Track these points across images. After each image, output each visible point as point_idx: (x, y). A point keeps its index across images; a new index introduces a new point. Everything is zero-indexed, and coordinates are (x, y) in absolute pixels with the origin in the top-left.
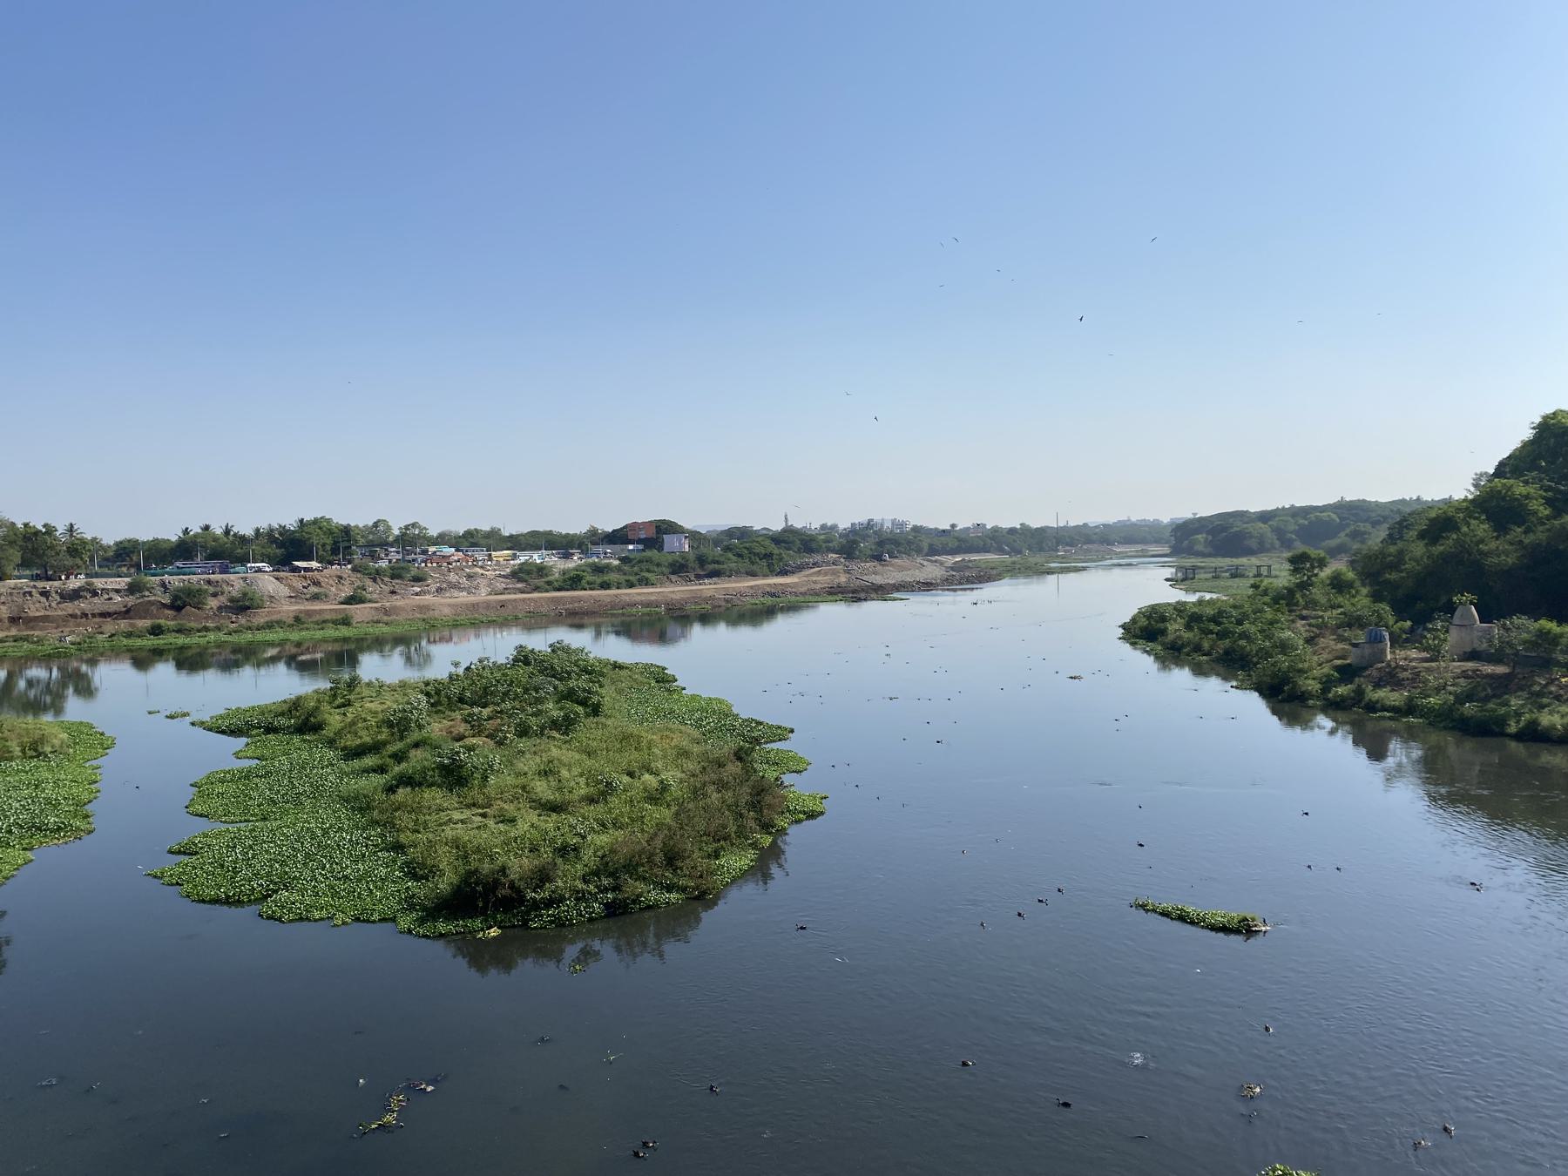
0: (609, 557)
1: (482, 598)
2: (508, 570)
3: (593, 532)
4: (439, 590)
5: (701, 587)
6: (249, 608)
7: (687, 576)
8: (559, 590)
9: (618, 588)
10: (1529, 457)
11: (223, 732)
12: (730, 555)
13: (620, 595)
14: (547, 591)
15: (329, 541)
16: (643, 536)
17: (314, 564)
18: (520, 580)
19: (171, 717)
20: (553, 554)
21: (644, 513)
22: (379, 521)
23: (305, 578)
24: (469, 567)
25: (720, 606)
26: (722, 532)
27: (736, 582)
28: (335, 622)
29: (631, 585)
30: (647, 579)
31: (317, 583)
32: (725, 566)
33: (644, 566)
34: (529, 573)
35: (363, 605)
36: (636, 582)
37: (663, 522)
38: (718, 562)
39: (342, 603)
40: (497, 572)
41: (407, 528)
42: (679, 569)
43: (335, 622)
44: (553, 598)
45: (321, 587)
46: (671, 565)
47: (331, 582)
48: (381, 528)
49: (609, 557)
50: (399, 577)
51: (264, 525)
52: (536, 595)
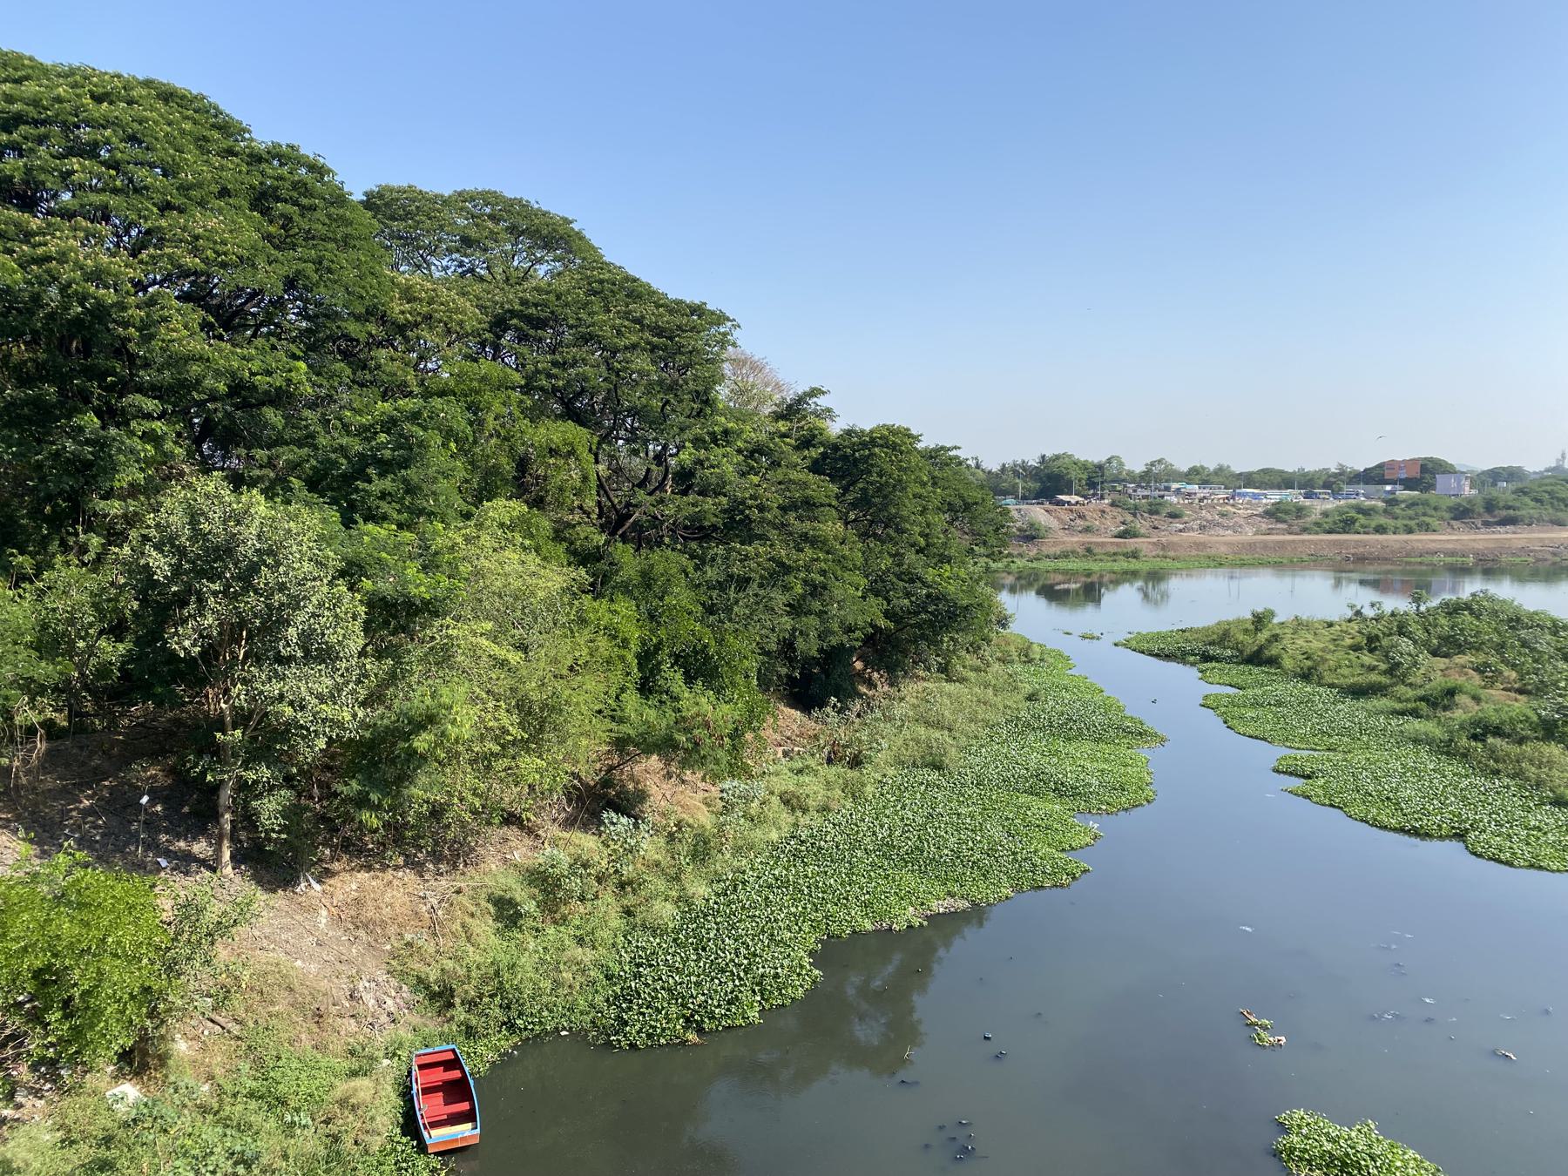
0: (1363, 496)
1: (1247, 538)
2: (1261, 510)
3: (1342, 472)
4: (1202, 528)
5: (1509, 536)
6: (1035, 538)
7: (1473, 523)
8: (1330, 532)
9: (1394, 533)
10: (671, 311)
11: (1157, 656)
12: (1527, 500)
13: (1411, 541)
14: (1317, 533)
15: (1085, 476)
16: (1403, 476)
17: (1074, 498)
18: (1279, 520)
19: (1084, 637)
20: (1300, 494)
21: (1404, 449)
22: (1113, 457)
23: (1071, 511)
24: (1221, 505)
25: (1546, 560)
26: (1483, 473)
27: (1540, 532)
28: (1126, 555)
29: (1410, 531)
30: (1428, 525)
31: (1082, 517)
32: (1523, 512)
33: (1420, 509)
34: (1287, 512)
35: (1136, 540)
36: (1415, 527)
37: (1431, 460)
38: (1509, 508)
39: (1116, 537)
40: (1249, 511)
41: (1152, 464)
42: (1462, 513)
43: (1126, 555)
44: (1336, 540)
45: (1086, 520)
46: (1450, 509)
47: (1095, 516)
48: (1114, 464)
49: (1363, 496)
50: (1157, 513)
51: (1009, 461)
52: (1306, 537)
